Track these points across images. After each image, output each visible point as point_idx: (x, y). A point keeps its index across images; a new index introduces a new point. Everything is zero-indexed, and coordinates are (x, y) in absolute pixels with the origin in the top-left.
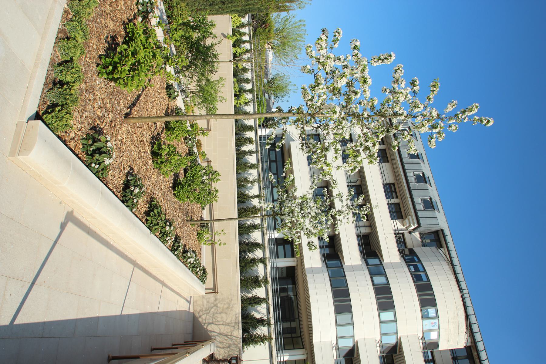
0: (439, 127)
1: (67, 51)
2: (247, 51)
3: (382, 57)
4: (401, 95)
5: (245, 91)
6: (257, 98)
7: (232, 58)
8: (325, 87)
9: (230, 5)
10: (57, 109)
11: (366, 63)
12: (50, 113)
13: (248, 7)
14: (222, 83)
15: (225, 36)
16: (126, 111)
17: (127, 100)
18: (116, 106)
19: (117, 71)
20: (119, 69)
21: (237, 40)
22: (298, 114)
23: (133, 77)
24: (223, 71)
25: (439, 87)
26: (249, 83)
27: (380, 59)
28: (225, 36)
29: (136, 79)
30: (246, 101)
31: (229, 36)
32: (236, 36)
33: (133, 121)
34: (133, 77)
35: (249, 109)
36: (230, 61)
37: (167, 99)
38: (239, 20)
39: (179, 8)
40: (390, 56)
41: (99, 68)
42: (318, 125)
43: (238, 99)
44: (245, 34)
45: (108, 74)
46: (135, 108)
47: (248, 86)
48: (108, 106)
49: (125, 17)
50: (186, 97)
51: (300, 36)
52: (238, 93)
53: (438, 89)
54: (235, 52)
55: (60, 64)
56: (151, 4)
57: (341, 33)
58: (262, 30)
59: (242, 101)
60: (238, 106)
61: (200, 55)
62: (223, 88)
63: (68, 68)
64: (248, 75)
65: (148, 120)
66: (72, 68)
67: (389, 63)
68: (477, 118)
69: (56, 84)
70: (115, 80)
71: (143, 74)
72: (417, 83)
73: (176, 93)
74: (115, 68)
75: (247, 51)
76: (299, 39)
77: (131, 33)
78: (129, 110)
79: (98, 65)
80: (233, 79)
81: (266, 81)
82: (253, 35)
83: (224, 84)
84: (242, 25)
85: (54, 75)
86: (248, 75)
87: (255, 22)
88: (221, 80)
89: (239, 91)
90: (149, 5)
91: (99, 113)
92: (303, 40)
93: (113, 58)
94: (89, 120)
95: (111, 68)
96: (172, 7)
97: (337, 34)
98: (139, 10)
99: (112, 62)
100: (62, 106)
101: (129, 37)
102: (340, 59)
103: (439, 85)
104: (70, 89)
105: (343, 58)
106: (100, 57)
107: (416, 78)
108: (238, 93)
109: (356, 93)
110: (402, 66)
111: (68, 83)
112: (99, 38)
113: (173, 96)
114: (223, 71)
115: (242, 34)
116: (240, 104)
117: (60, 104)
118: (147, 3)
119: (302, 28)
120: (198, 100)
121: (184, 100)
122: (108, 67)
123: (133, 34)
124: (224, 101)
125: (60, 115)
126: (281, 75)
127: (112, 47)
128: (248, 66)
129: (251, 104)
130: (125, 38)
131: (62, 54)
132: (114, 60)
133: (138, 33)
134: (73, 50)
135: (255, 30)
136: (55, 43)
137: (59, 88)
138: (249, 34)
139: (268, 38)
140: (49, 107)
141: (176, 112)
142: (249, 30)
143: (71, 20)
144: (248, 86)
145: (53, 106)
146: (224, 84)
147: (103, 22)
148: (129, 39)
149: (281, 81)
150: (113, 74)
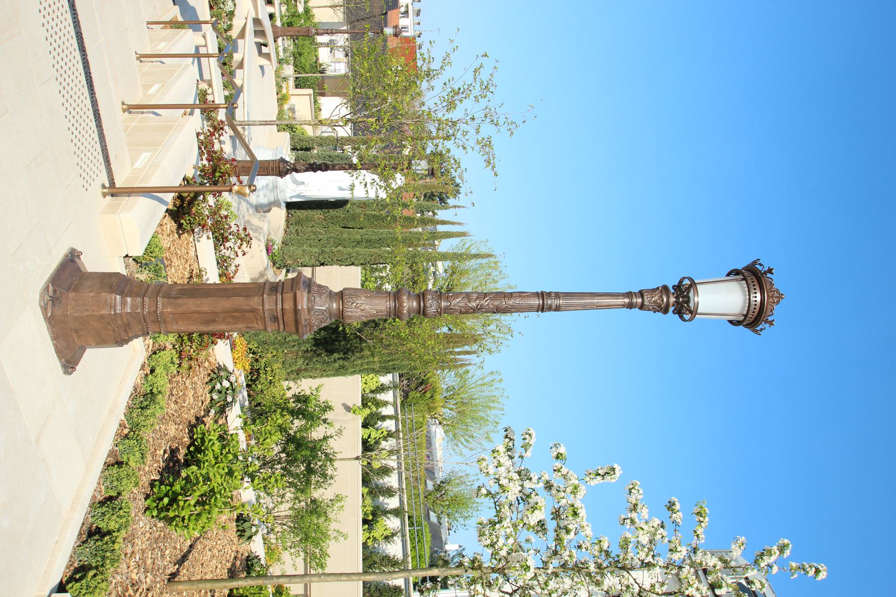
0: (724, 584)
1: (115, 483)
2: (390, 434)
3: (601, 472)
4: (641, 532)
5: (386, 512)
6: (411, 524)
7: (360, 454)
8: (510, 525)
9: (359, 362)
10: (91, 573)
11: (576, 482)
12: (77, 581)
13: (391, 363)
14: (339, 504)
15: (348, 409)
16: (172, 569)
17: (175, 548)
18: (159, 562)
19: (175, 507)
20: (181, 503)
21: (372, 415)
22: (473, 569)
23: (199, 515)
24: (344, 483)
25: (709, 516)
26: (393, 496)
27: (599, 475)
28: (348, 409)
29: (204, 518)
30: (387, 533)
31: (355, 407)
32: (369, 408)
33: (180, 587)
34: (199, 515)
35: (394, 549)
36: (357, 458)
37: (236, 540)
38: (375, 379)
39: (269, 372)
40: (613, 469)
41: (149, 501)
42: (515, 588)
43: (370, 529)
44: (385, 404)
45: (160, 510)
46: (186, 563)
47: (392, 503)
48: (149, 562)
49: (190, 417)
50: (268, 533)
51: (493, 399)
52: (370, 518)
53: (707, 519)
54: (366, 437)
55: (102, 503)
56: (233, 390)
57: (534, 435)
58: (418, 395)
59: (378, 532)
60: (370, 543)
61: (303, 459)
62: (342, 512)
63: (114, 509)
64: (392, 481)
65: (201, 586)
66: (120, 509)
67: (613, 481)
68: (794, 564)
69: (93, 534)
70: (169, 521)
71: (217, 509)
72: (677, 507)
73: (254, 529)
74: (174, 500)
75: (390, 434)
76: (492, 405)
77: (199, 440)
78: (177, 566)
79: (147, 497)
80: (360, 490)
81: (430, 485)
82: (402, 404)
83: (342, 506)
84: (382, 389)
85: (91, 520)
86: (392, 481)
87: (405, 382)
88: (338, 498)
89: (374, 514)
90: (230, 391)
91: (134, 576)
92: (500, 406)
93: (171, 485)
94: (119, 589)
95: (166, 500)
96: (258, 371)
97: (527, 436)
98: (212, 399)
99: (170, 493)
100: (97, 568)
101: (194, 445)
102: (531, 479)
103: (707, 511)
104: (114, 542)
105: (537, 477)
106: (152, 484)
107: (674, 499)
108: (370, 518)
109: (568, 531)
110: (638, 483)
111: (109, 533)
112: (154, 455)
113: (247, 534)
114: (344, 483)
115: (378, 404)
116: (375, 539)
117: (94, 565)
118: (227, 389)
119: (496, 385)
120: (291, 538)
121: (264, 539)
122: (161, 499)
123: (203, 439)
124: (341, 539)
125: (93, 584)
126: (460, 474)
127: (172, 466)
128: (392, 463)
129: (398, 540)
130: (188, 448)
131: (107, 487)
132: (174, 489)
133: (210, 440)
134: (125, 481)
135: (406, 396)
136: (102, 472)
137: (97, 540)
138: (395, 405)
139: (430, 409)
140: (77, 571)
141: (249, 564)
142: (395, 396)
143: (126, 437)
144: (392, 503)
145: (83, 569)
146: (342, 506)
147: (163, 428)
148: (196, 450)
149: (463, 487)
150: (168, 510)
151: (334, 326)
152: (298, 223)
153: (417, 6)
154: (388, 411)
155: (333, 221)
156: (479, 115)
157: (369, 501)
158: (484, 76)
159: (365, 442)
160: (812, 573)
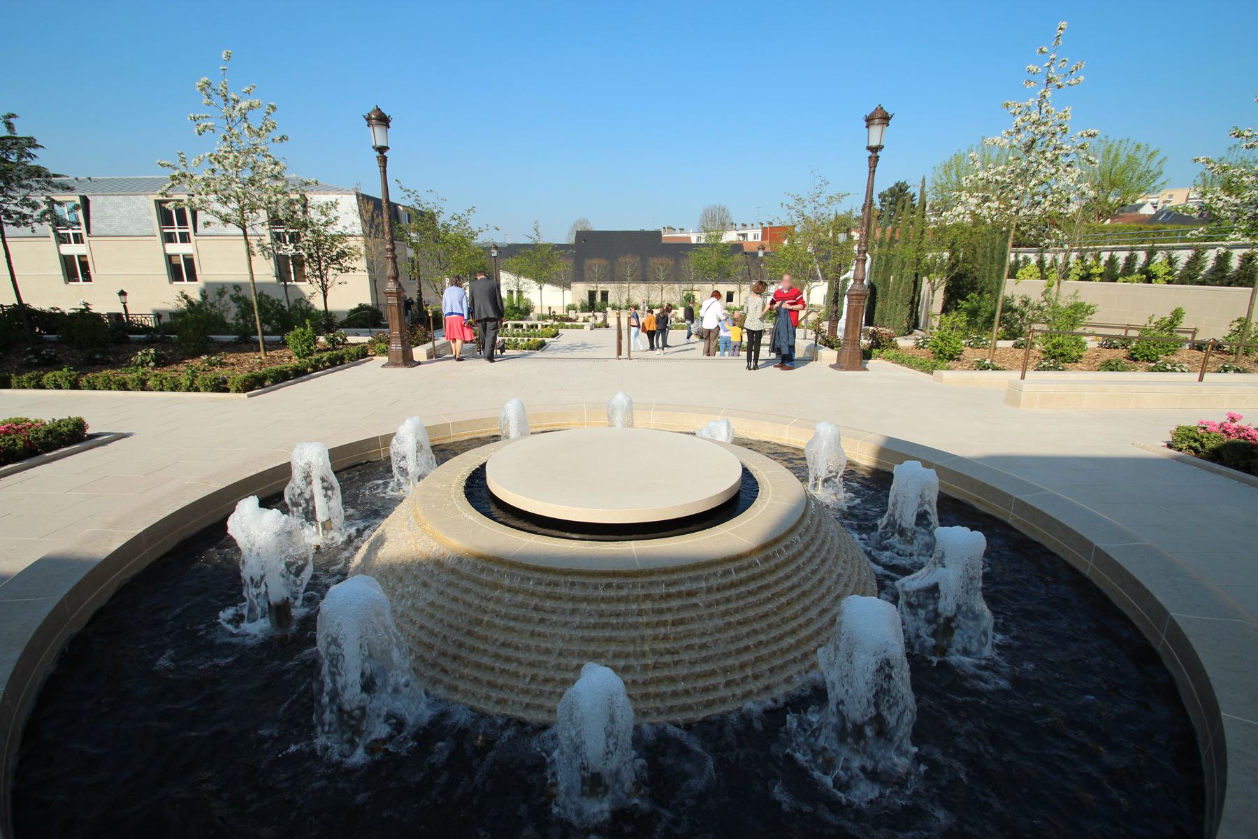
2: (1082, 258)
35: (1183, 257)
43: (1155, 277)
47: (1142, 257)
64: (1122, 256)
128: (1105, 256)
129: (1175, 254)
151: (371, 207)
152: (883, 319)
153: (739, 226)
154: (1060, 258)
155: (885, 294)
156: (813, 205)
157: (1134, 277)
158: (792, 203)
159: (1082, 279)
160: (1060, 32)
